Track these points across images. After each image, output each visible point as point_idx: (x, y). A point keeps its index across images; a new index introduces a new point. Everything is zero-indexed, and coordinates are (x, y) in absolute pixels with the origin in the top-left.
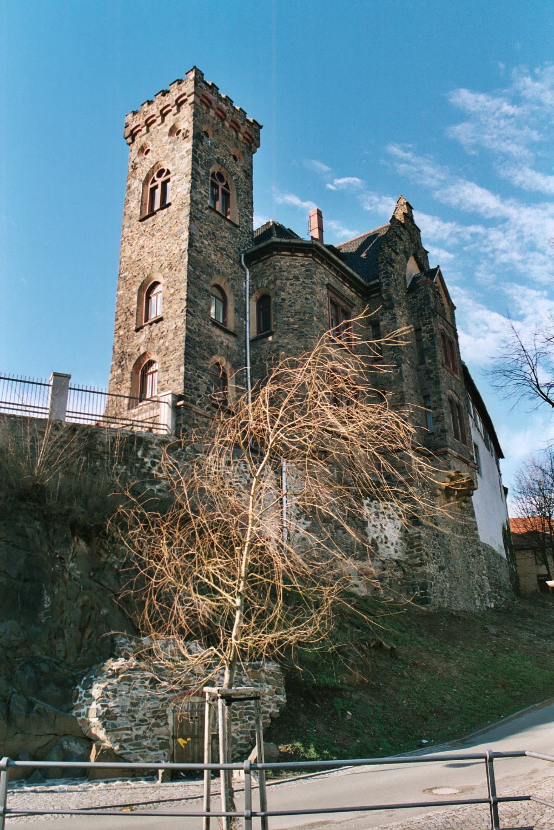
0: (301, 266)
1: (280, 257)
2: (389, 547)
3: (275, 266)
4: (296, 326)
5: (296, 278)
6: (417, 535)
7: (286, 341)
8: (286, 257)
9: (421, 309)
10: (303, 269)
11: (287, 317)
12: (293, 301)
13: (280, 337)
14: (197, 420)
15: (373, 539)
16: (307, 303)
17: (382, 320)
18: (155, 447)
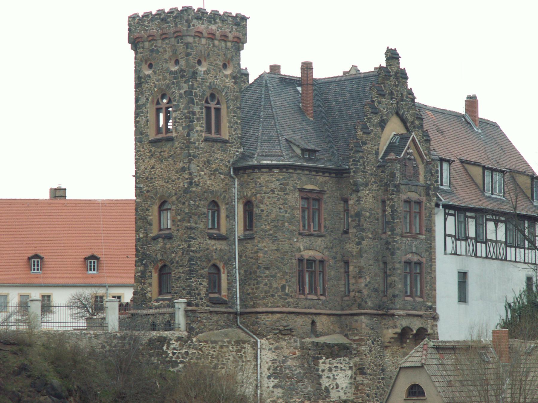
0: (277, 180)
1: (260, 173)
2: (339, 391)
3: (256, 181)
4: (271, 232)
5: (273, 191)
6: (361, 382)
7: (264, 245)
8: (265, 174)
9: (387, 185)
10: (278, 183)
11: (265, 225)
12: (269, 211)
13: (259, 242)
14: (200, 317)
15: (326, 387)
16: (280, 212)
17: (350, 200)
18: (174, 342)
